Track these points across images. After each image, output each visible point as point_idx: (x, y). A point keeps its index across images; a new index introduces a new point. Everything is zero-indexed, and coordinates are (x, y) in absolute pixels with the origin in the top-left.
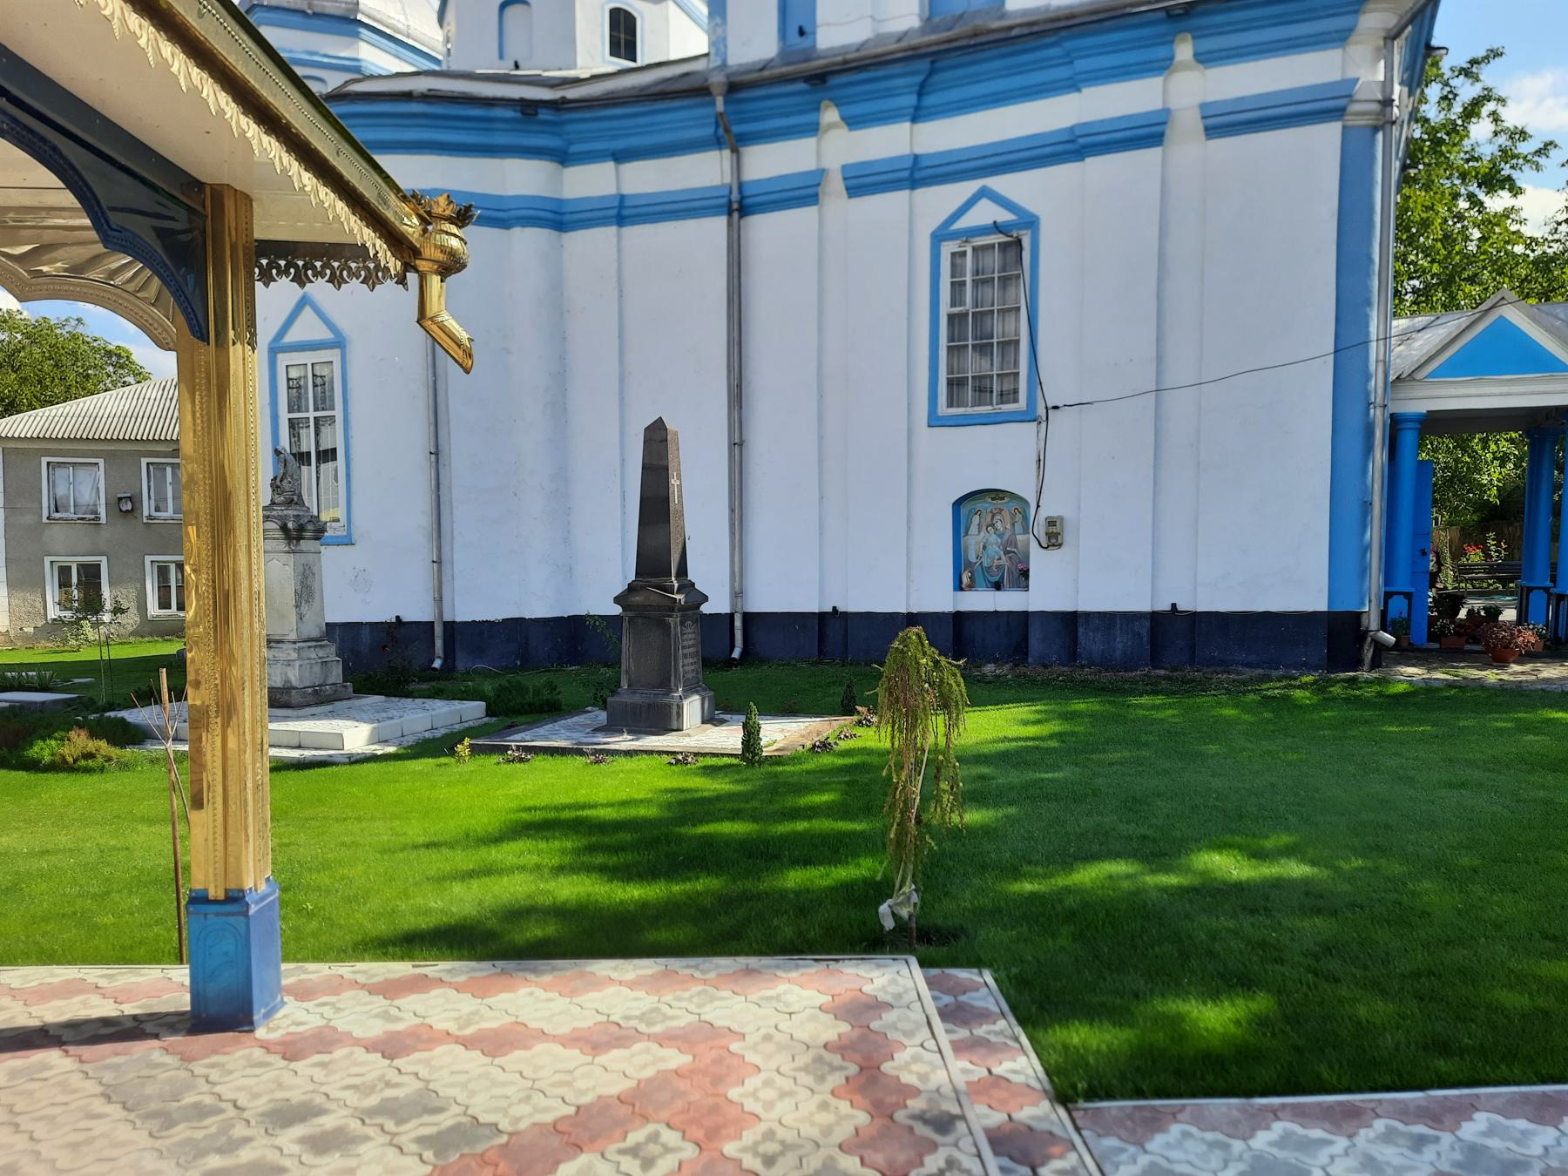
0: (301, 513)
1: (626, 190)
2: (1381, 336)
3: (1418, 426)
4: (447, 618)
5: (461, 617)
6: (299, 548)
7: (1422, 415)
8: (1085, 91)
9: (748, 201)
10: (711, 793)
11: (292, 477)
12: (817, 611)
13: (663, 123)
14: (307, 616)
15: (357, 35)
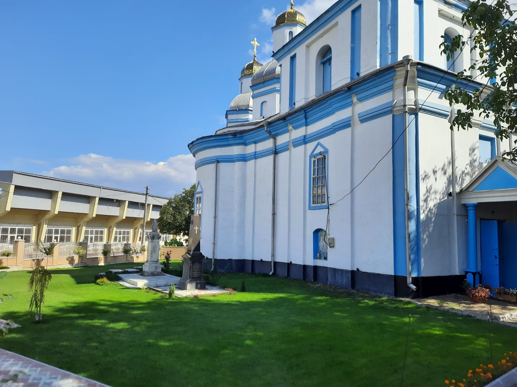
0: (154, 233)
1: (257, 150)
3: (474, 208)
4: (215, 258)
5: (218, 258)
6: (153, 241)
7: (475, 204)
8: (336, 113)
9: (277, 151)
10: (115, 302)
11: (155, 226)
12: (287, 262)
13: (260, 134)
15: (248, 113)
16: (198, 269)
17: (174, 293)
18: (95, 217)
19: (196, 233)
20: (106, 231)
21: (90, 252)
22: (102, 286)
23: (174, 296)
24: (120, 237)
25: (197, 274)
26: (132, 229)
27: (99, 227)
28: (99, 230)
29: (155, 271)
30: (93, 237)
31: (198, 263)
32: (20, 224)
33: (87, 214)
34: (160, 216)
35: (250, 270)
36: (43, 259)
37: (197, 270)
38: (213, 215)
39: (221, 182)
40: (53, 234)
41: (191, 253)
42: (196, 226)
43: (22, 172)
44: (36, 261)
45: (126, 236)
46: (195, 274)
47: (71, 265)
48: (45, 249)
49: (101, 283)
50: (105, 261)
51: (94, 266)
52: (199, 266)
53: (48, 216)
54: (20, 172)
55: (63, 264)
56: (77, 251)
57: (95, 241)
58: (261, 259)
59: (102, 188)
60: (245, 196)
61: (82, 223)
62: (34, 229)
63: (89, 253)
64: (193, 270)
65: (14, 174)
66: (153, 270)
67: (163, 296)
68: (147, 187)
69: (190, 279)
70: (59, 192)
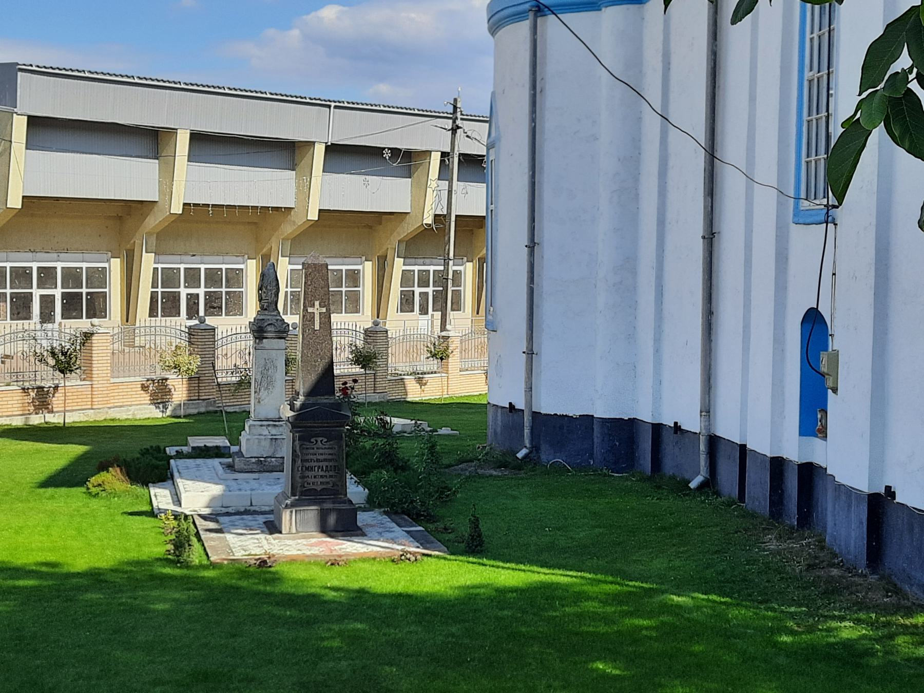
14: (266, 401)
16: (325, 460)
17: (190, 545)
18: (317, 221)
19: (317, 327)
20: (368, 270)
23: (195, 556)
24: (427, 294)
25: (321, 480)
26: (472, 261)
28: (344, 268)
29: (270, 454)
32: (67, 251)
33: (289, 209)
36: (56, 388)
37: (321, 464)
39: (552, 99)
40: (179, 287)
41: (298, 404)
42: (317, 303)
43: (45, 67)
44: (33, 394)
46: (313, 480)
47: (159, 408)
48: (53, 354)
52: (330, 451)
53: (153, 222)
54: (38, 66)
55: (130, 406)
58: (676, 423)
59: (336, 107)
61: (274, 244)
62: (115, 267)
63: (224, 364)
64: (307, 465)
65: (19, 74)
68: (455, 100)
69: (297, 497)
70: (179, 131)
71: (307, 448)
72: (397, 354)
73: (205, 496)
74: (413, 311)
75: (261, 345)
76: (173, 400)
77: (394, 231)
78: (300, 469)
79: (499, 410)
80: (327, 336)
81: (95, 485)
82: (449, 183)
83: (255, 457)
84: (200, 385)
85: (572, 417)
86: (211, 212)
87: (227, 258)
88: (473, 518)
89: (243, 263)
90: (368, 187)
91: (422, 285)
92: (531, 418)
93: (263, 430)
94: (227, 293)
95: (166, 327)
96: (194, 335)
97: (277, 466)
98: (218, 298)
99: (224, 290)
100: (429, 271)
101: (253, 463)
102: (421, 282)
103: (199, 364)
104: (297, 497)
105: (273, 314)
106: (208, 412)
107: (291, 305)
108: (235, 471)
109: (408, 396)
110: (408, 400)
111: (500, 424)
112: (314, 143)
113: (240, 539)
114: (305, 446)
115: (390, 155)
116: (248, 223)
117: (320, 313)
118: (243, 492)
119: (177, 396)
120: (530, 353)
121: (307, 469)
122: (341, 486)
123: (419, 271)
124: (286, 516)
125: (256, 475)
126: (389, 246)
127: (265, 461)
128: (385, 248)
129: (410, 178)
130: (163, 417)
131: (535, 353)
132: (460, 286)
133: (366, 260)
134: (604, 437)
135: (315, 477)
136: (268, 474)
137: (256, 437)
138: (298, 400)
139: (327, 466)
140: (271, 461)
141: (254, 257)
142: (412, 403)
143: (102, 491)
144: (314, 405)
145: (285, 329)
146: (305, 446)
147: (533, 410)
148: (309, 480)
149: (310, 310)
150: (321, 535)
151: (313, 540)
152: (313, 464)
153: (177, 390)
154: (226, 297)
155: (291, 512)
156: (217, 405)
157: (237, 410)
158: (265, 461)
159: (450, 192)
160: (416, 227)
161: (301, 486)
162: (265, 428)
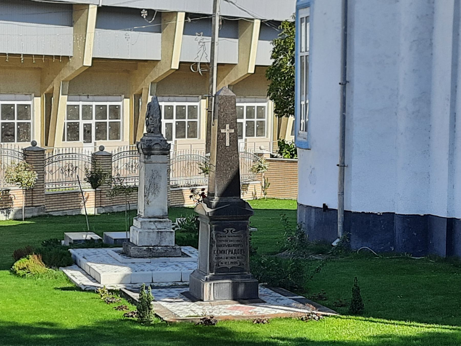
2: (31, 200)
11: (152, 116)
14: (153, 203)
16: (234, 245)
17: (150, 309)
19: (228, 144)
21: (54, 178)
22: (18, 280)
24: (171, 124)
25: (232, 260)
27: (107, 94)
28: (108, 104)
29: (157, 244)
30: (91, 124)
31: (234, 230)
34: (273, 60)
35: (441, 249)
37: (231, 248)
38: (338, 79)
41: (214, 202)
42: (228, 126)
45: (186, 120)
46: (226, 260)
47: (3, 212)
49: (21, 272)
50: (98, 204)
51: (66, 215)
56: (14, 175)
57: (97, 138)
60: (433, 13)
63: (50, 178)
64: (221, 249)
66: (152, 240)
67: (131, 314)
69: (214, 274)
71: (221, 237)
72: (177, 170)
73: (118, 275)
74: (78, 139)
75: (149, 160)
76: (14, 206)
77: (148, 75)
78: (216, 252)
79: (314, 210)
80: (234, 151)
81: (20, 268)
82: (212, 39)
83: (146, 246)
84: (34, 195)
85: (376, 214)
86: (22, 59)
87: (18, 96)
88: (355, 288)
89: (31, 100)
90: (129, 40)
91: (167, 118)
92: (343, 215)
93: (152, 225)
94: (18, 124)
95: (8, 149)
96: (28, 156)
97: (162, 253)
98: (11, 128)
99: (16, 121)
100: (172, 106)
101: (145, 250)
102: (166, 115)
103: (37, 178)
104: (214, 274)
105: (157, 135)
106: (40, 216)
107: (67, 133)
108: (130, 256)
109: (185, 203)
110: (185, 206)
111: (314, 220)
112: (88, 5)
113: (173, 305)
114: (219, 235)
115: (146, 15)
116: (35, 68)
117: (230, 133)
118: (145, 272)
119: (16, 203)
120: (342, 166)
121: (221, 252)
122: (246, 264)
123: (165, 106)
124: (207, 287)
125: (148, 260)
126: (144, 87)
127: (153, 249)
128: (140, 88)
129: (160, 32)
130: (6, 220)
131: (346, 165)
132: (197, 118)
133: (125, 98)
134: (404, 230)
135: (227, 258)
136: (156, 259)
137: (146, 230)
138: (214, 200)
139: (235, 250)
140: (158, 248)
141: (39, 95)
142: (188, 208)
143: (28, 273)
144: (226, 203)
145: (167, 147)
146: (219, 235)
147: (345, 210)
148: (222, 261)
149: (223, 131)
150: (233, 302)
151: (229, 306)
152: (225, 248)
153: (16, 198)
154: (17, 127)
155: (211, 285)
156: (46, 211)
157: (61, 214)
158: (153, 249)
159: (213, 44)
160: (165, 72)
161: (216, 265)
162: (152, 223)
